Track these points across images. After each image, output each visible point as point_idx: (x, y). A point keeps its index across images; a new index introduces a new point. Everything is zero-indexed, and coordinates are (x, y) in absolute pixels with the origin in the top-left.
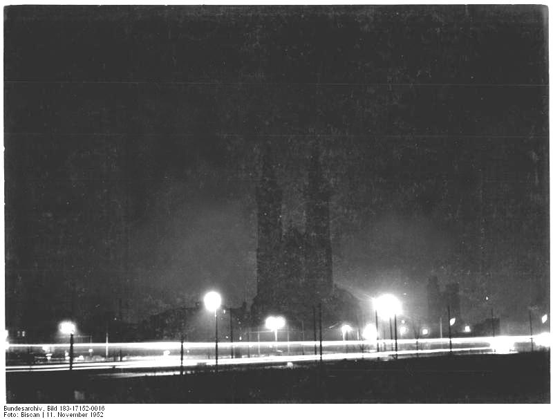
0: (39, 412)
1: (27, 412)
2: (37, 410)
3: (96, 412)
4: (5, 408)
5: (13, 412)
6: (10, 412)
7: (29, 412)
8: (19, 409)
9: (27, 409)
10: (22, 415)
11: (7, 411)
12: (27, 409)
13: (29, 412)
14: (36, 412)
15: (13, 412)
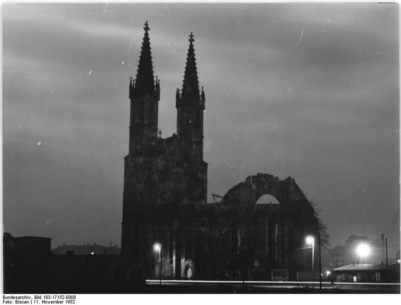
0: (28, 300)
1: (20, 300)
2: (27, 298)
3: (70, 300)
4: (4, 297)
5: (10, 300)
6: (7, 300)
7: (21, 300)
8: (14, 298)
9: (20, 298)
10: (16, 302)
11: (5, 299)
12: (20, 298)
13: (21, 300)
14: (26, 300)
15: (10, 300)
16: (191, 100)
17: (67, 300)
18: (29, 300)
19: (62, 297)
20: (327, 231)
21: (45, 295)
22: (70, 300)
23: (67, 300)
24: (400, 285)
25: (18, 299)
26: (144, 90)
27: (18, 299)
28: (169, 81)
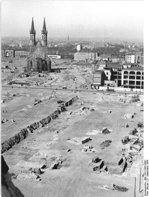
0: (146, 183)
1: (147, 187)
2: (146, 184)
3: (146, 162)
6: (147, 194)
8: (145, 190)
11: (146, 194)
14: (147, 184)
15: (146, 192)
16: (45, 32)
17: (146, 164)
18: (147, 182)
19: (145, 166)
20: (42, 30)
21: (148, 191)
22: (146, 162)
23: (146, 164)
24: (121, 76)
25: (146, 188)
26: (33, 32)
27: (146, 188)
28: (39, 29)
